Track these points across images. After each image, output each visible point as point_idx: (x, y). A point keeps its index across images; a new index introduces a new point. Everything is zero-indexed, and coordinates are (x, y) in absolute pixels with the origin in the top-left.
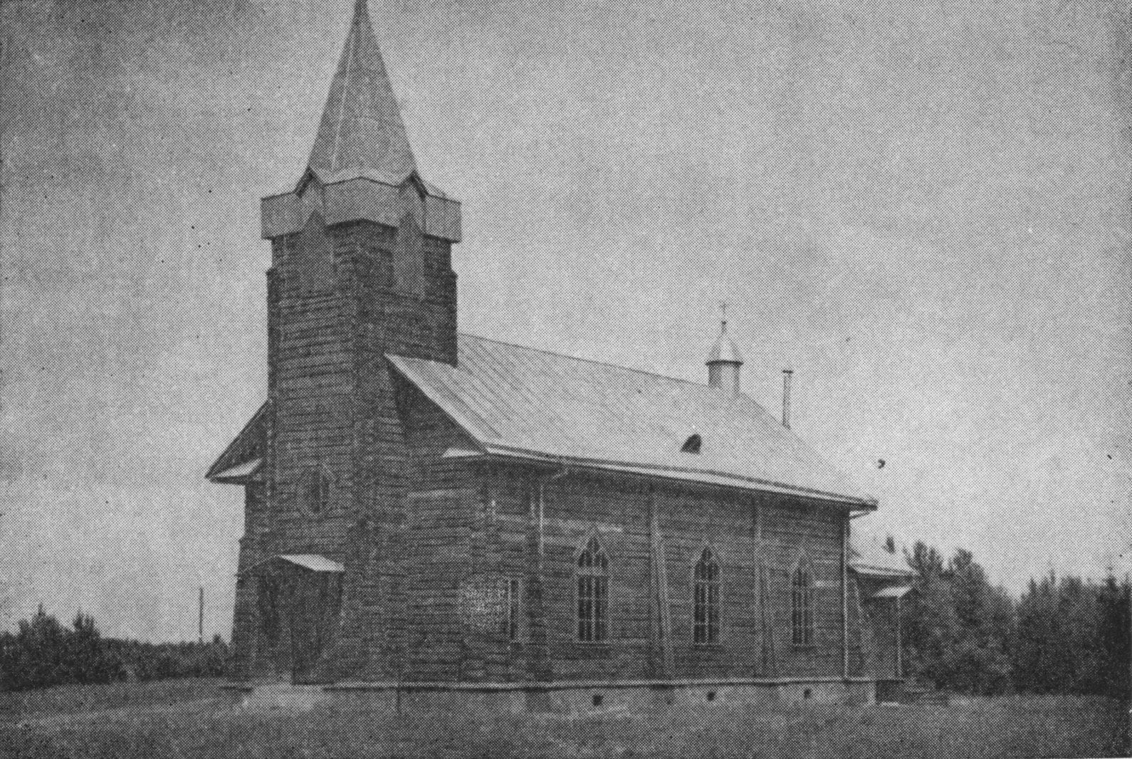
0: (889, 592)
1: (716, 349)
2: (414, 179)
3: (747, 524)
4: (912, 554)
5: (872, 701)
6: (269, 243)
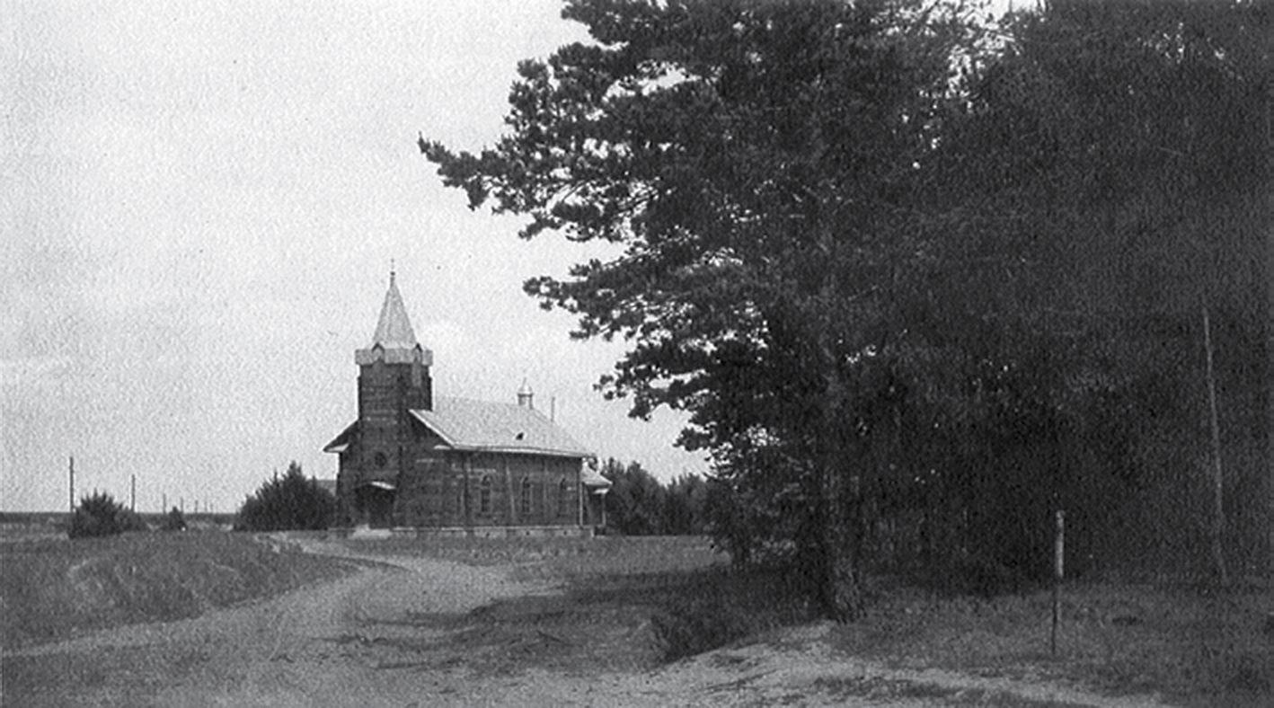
0: (598, 491)
1: (522, 389)
2: (418, 346)
3: (541, 466)
4: (607, 463)
5: (592, 535)
6: (358, 367)
